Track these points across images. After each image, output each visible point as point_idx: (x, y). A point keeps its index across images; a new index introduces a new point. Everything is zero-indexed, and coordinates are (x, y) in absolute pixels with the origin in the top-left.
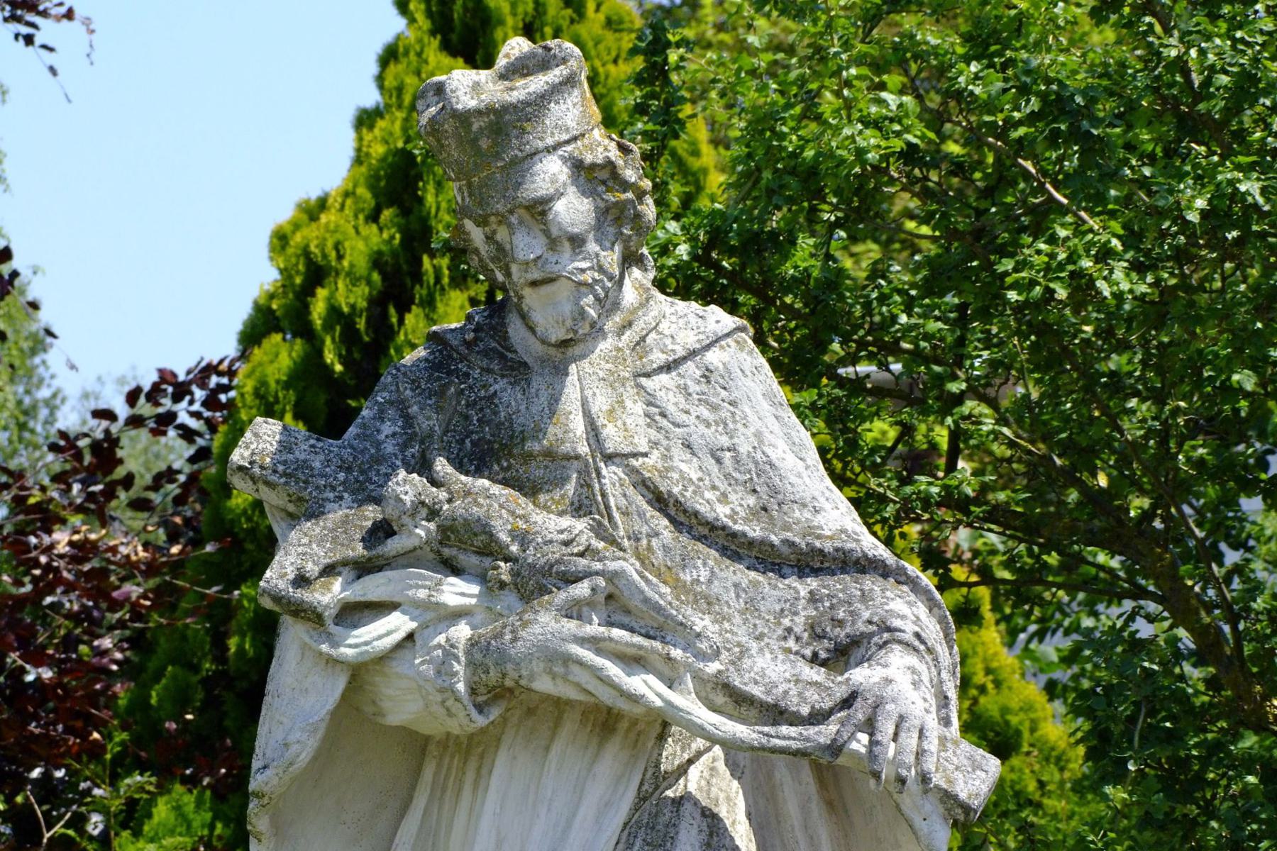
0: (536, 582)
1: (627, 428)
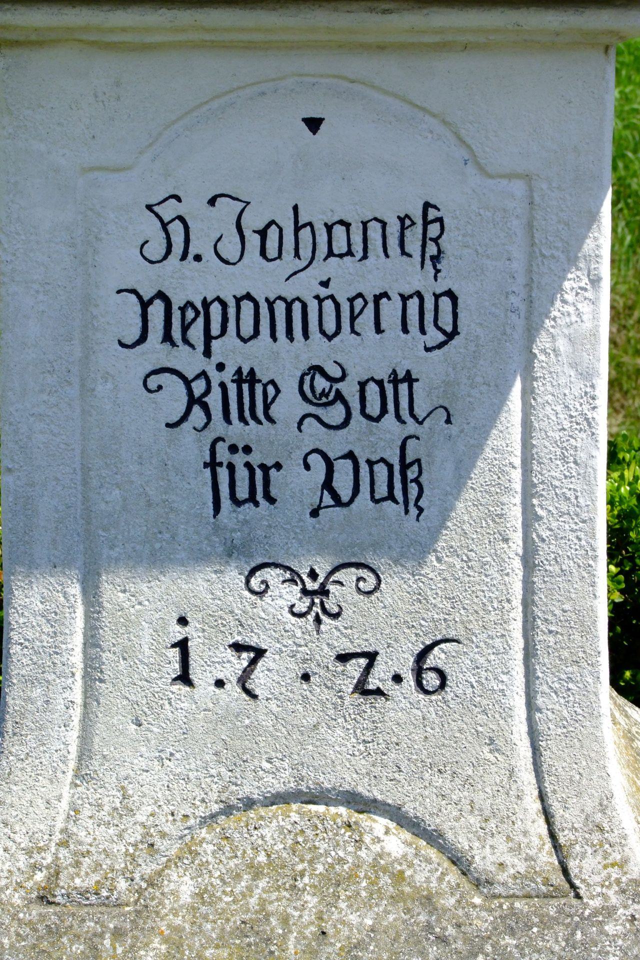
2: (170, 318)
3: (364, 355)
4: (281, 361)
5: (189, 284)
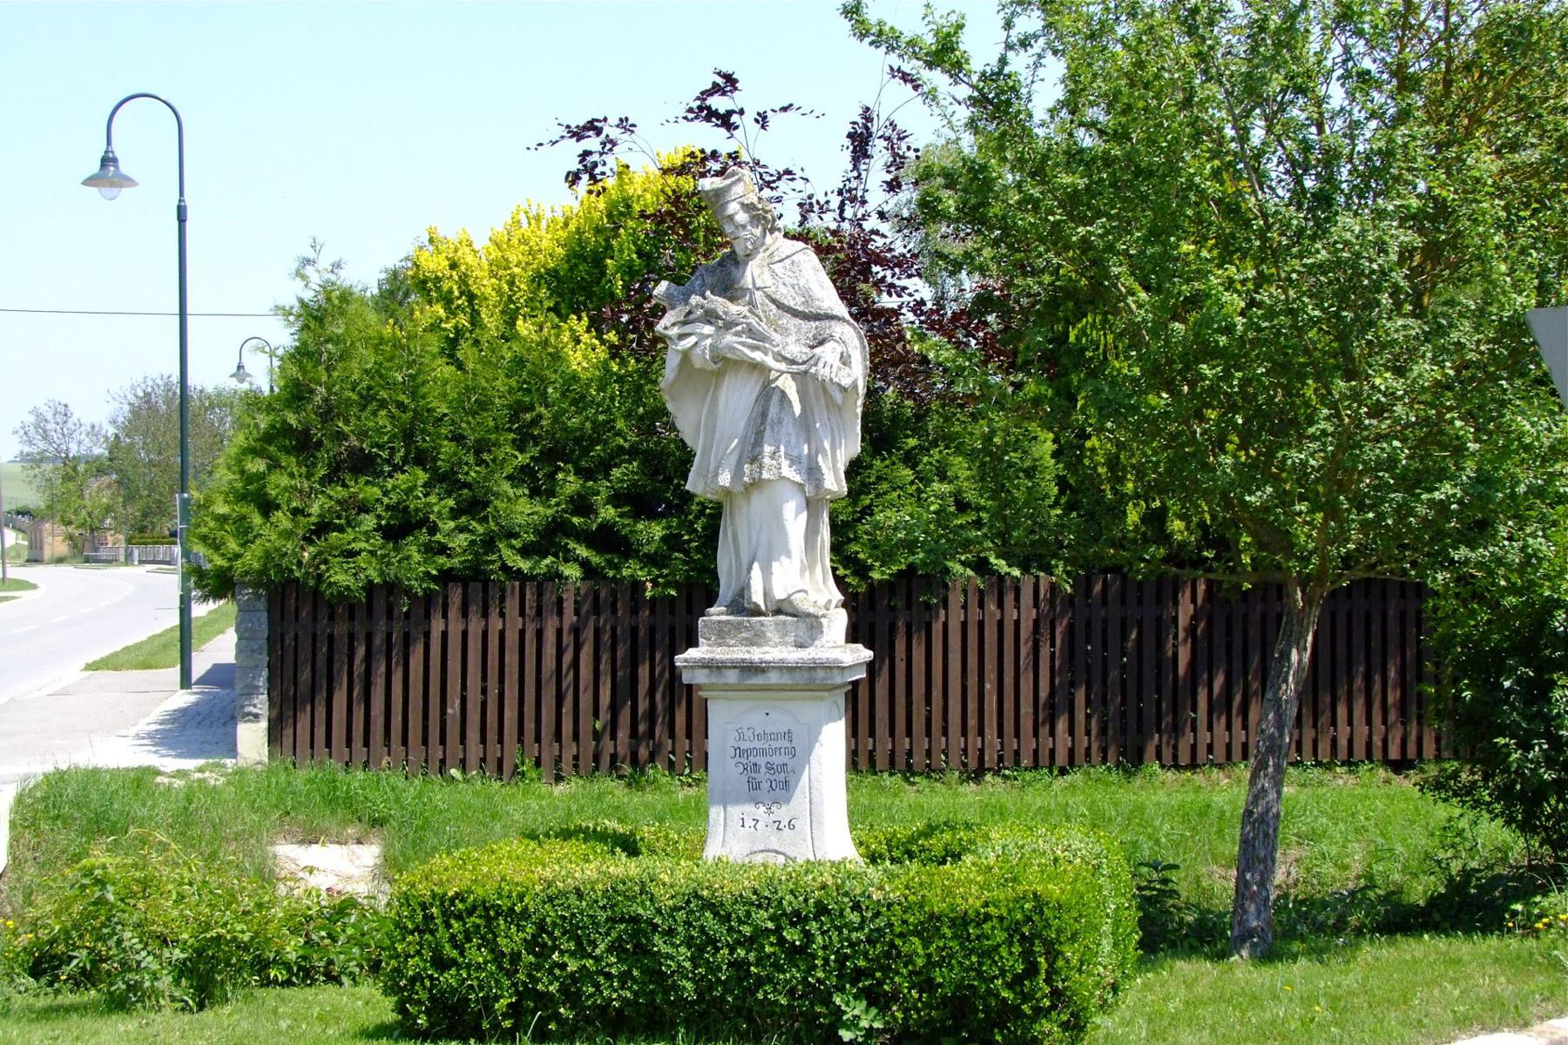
0: (729, 325)
1: (765, 280)
2: (740, 752)
3: (778, 760)
4: (761, 761)
5: (744, 745)
